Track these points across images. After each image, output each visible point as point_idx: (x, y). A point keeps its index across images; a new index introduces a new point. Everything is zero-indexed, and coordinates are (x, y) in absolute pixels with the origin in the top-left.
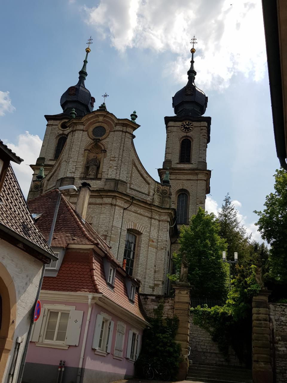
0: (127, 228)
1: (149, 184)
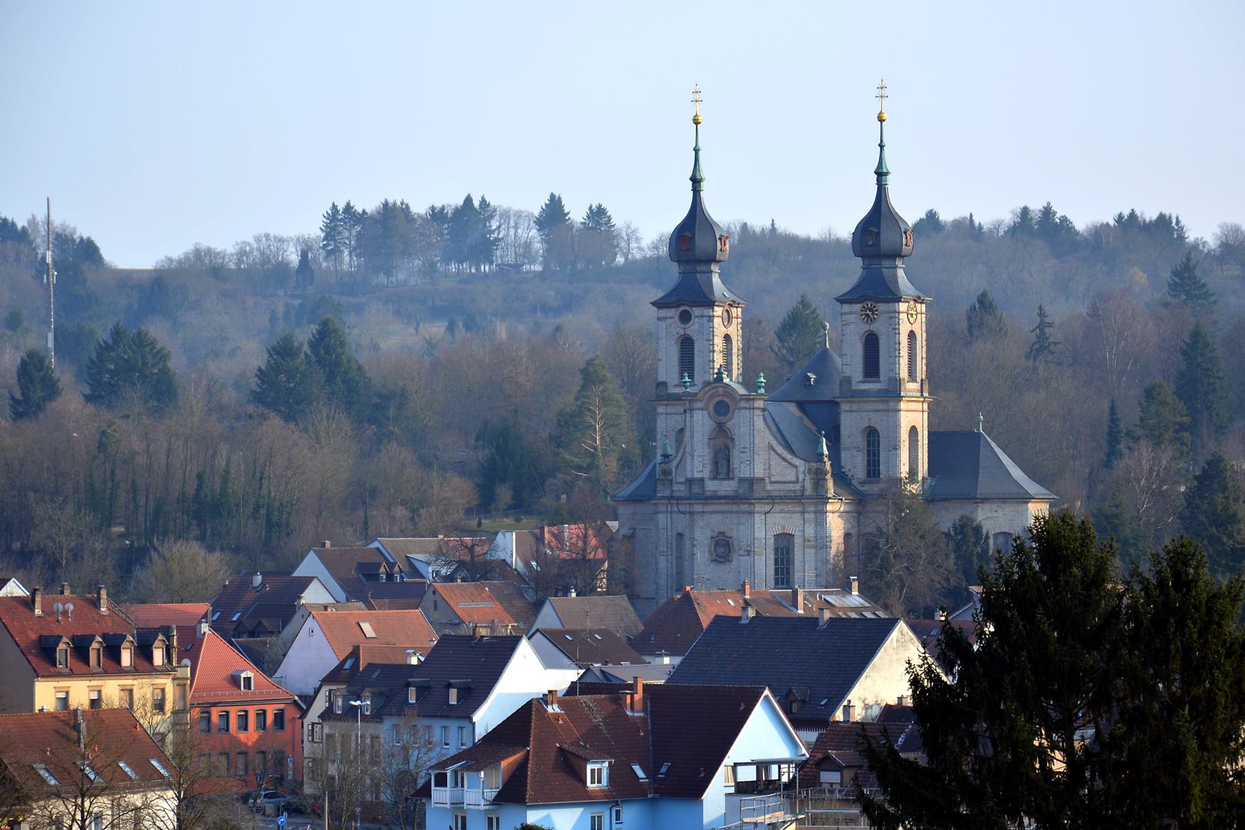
1: (796, 467)
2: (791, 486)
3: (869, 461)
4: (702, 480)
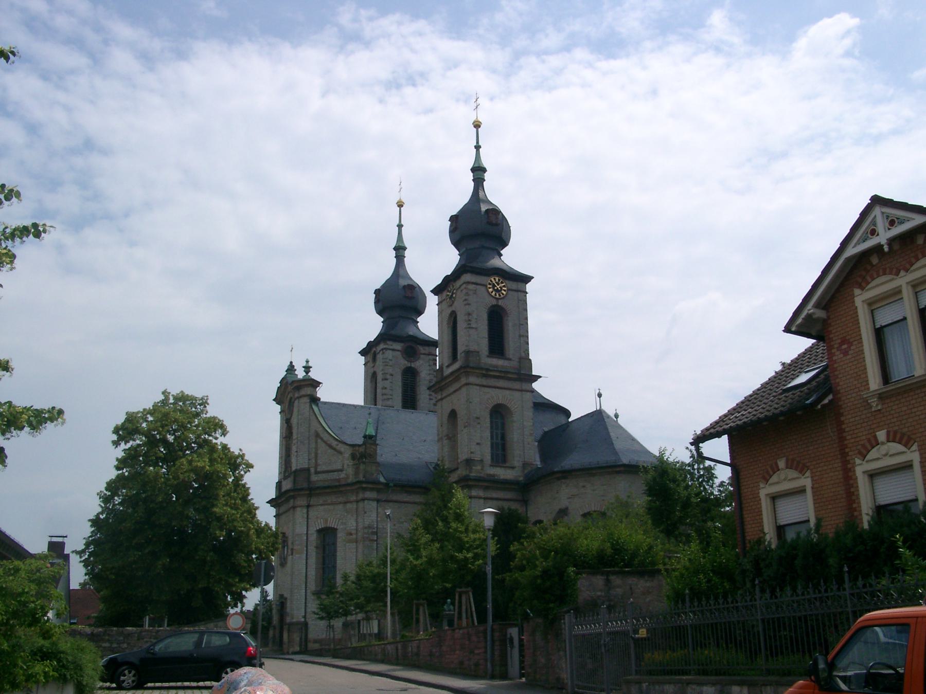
0: (315, 529)
1: (340, 453)
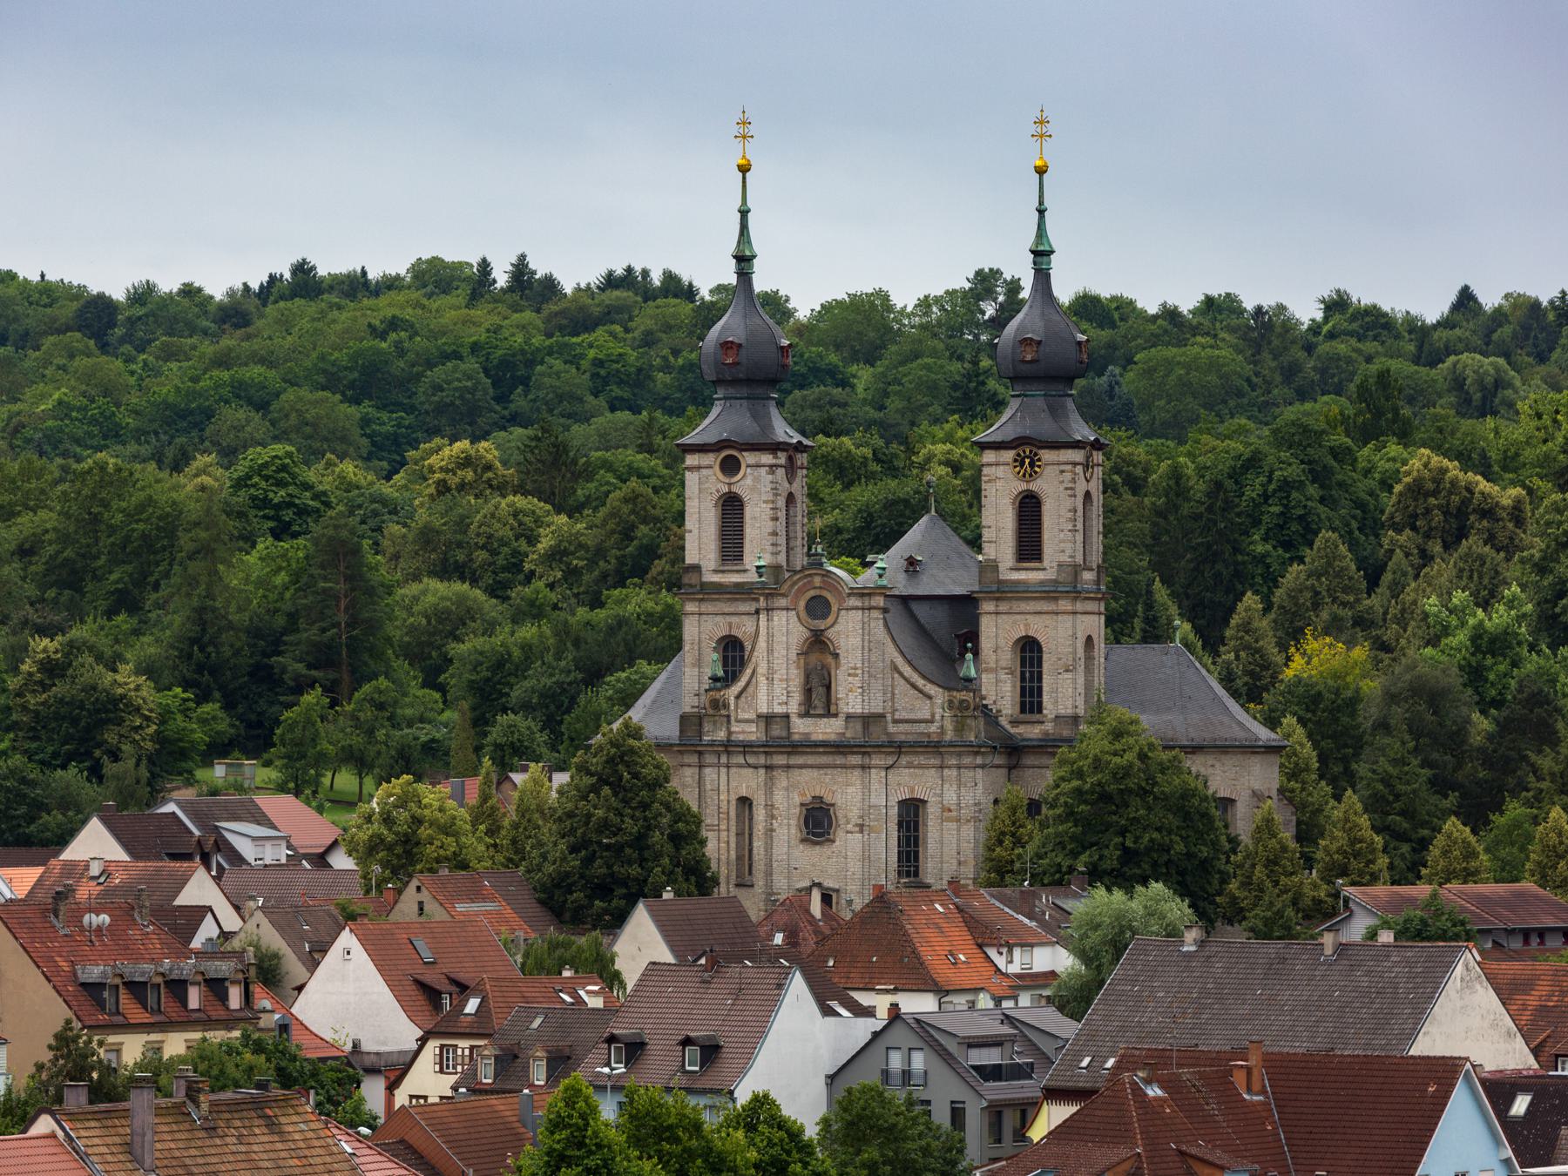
1: (930, 697)
2: (922, 728)
3: (1023, 689)
4: (787, 716)
